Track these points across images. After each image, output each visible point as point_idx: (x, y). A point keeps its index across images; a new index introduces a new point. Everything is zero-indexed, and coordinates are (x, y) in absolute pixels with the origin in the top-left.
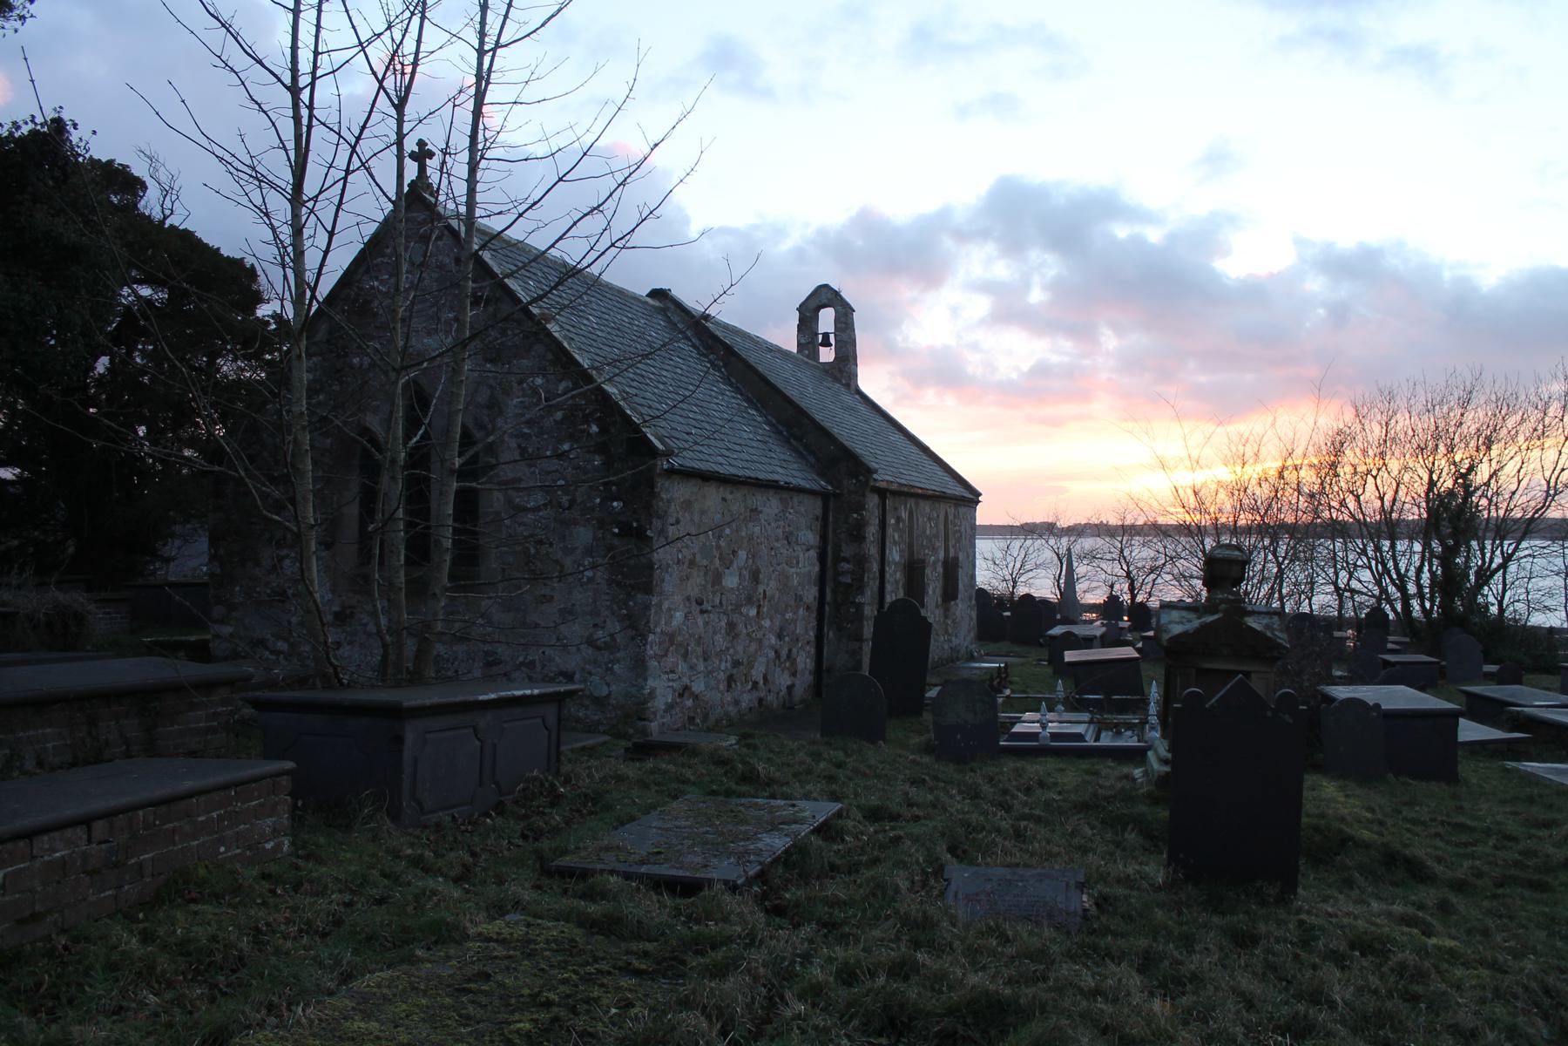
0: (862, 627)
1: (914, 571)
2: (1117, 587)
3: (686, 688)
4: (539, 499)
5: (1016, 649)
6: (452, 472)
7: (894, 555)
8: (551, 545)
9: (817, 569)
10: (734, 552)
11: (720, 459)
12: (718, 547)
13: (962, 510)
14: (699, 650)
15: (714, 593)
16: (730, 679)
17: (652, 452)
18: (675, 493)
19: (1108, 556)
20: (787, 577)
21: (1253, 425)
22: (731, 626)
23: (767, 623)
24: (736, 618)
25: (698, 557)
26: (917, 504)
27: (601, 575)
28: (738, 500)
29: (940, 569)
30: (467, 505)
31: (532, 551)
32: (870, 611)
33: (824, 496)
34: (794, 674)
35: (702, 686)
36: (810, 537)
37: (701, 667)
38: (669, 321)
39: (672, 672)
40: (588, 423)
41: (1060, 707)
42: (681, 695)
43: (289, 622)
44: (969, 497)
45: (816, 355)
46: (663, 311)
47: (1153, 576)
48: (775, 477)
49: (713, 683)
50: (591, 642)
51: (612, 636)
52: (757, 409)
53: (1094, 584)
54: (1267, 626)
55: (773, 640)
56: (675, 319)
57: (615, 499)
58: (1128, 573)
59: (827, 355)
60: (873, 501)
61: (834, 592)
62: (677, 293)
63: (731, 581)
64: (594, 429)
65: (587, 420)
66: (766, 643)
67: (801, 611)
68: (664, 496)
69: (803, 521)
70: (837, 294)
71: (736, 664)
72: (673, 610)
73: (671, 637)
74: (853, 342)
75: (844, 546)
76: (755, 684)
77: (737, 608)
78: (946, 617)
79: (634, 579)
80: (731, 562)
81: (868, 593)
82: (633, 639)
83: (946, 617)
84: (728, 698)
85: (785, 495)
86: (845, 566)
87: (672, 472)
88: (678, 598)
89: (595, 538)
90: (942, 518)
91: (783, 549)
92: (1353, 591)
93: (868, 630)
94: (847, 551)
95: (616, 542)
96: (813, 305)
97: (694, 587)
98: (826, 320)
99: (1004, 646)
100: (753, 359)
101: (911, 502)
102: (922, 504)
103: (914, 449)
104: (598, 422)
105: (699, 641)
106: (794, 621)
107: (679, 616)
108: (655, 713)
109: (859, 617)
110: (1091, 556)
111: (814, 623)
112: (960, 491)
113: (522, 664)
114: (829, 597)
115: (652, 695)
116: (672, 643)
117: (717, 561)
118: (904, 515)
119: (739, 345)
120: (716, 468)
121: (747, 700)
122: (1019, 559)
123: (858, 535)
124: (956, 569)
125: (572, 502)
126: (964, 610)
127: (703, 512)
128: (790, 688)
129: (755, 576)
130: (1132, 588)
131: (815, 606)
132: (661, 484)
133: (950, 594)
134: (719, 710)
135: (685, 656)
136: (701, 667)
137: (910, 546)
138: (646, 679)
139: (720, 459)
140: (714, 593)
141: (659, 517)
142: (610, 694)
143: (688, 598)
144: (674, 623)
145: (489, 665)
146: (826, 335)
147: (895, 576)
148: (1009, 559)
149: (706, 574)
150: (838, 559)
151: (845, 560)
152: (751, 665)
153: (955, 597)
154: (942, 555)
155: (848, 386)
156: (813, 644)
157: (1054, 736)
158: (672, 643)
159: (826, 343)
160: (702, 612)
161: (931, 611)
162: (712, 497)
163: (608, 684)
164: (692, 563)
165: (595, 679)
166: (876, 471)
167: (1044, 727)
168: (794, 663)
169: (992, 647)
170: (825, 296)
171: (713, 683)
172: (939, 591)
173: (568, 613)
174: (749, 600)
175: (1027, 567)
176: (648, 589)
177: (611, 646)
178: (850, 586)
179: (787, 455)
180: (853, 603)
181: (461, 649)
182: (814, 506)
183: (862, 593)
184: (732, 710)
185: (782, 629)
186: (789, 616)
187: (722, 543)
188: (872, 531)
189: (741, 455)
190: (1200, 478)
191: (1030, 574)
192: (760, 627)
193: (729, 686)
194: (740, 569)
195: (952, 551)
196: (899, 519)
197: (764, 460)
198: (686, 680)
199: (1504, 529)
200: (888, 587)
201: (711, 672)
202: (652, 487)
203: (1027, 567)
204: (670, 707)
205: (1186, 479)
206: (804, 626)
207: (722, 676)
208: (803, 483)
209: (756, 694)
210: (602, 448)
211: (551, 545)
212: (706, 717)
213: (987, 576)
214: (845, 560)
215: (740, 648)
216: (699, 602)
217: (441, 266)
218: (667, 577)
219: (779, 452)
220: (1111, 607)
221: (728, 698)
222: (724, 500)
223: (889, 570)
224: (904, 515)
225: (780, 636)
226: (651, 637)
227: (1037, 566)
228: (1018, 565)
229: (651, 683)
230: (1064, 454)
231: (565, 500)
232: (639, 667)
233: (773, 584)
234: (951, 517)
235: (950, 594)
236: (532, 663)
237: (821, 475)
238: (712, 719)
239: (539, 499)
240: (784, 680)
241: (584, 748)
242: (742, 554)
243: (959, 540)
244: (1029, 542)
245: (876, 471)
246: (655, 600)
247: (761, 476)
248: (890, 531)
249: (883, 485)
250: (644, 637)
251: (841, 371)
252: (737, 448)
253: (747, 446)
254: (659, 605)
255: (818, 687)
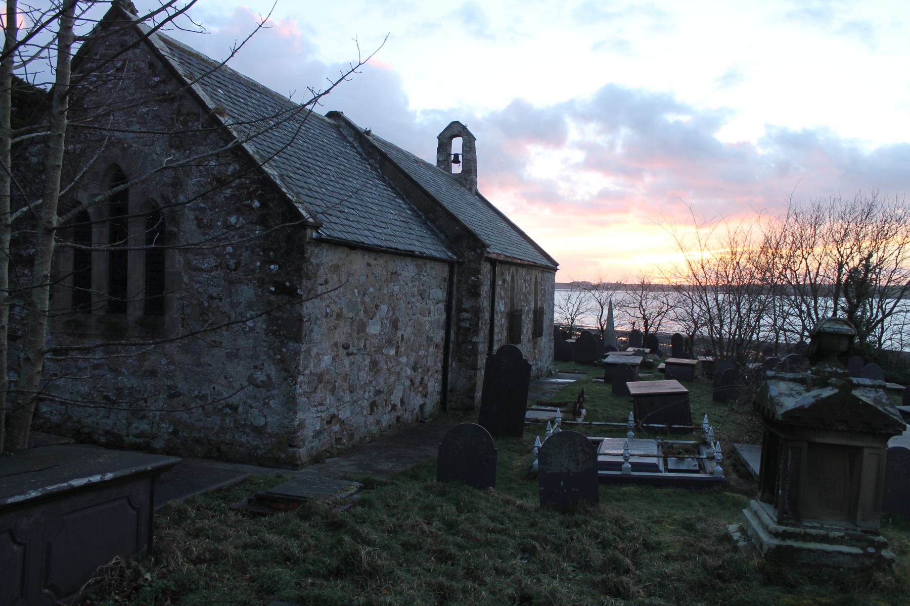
0: (476, 360)
1: (514, 318)
2: (637, 323)
3: (333, 416)
4: (211, 261)
5: (579, 367)
6: (7, 226)
7: (501, 306)
8: (220, 299)
9: (444, 317)
10: (377, 306)
11: (367, 233)
12: (363, 303)
13: (546, 275)
14: (346, 385)
15: (359, 339)
16: (373, 405)
17: (305, 225)
18: (324, 259)
19: (632, 305)
20: (421, 325)
21: (722, 230)
22: (374, 364)
23: (404, 360)
24: (378, 357)
25: (345, 311)
26: (517, 271)
27: (261, 325)
28: (380, 265)
29: (531, 316)
30: (156, 264)
31: (206, 304)
32: (482, 348)
33: (451, 264)
34: (425, 396)
35: (348, 414)
36: (440, 294)
37: (347, 398)
38: (341, 134)
39: (321, 404)
40: (252, 199)
41: (631, 433)
42: (329, 423)
43: (19, 358)
44: (552, 266)
45: (449, 169)
46: (337, 128)
47: (659, 317)
48: (412, 248)
49: (358, 409)
50: (251, 381)
51: (269, 377)
52: (403, 199)
53: (623, 322)
54: (875, 400)
55: (409, 372)
56: (345, 133)
57: (273, 263)
58: (644, 316)
59: (457, 169)
60: (486, 267)
61: (457, 334)
62: (347, 115)
63: (374, 329)
64: (256, 204)
65: (250, 196)
66: (403, 374)
67: (431, 349)
68: (313, 260)
69: (434, 281)
70: (464, 128)
71: (378, 393)
72: (321, 352)
73: (320, 377)
74: (475, 161)
75: (464, 300)
76: (394, 407)
77: (379, 350)
78: (535, 348)
79: (288, 330)
80: (374, 314)
81: (482, 335)
82: (285, 379)
83: (535, 348)
84: (371, 419)
85: (420, 262)
86: (465, 315)
87: (320, 241)
88: (326, 345)
89: (256, 295)
90: (533, 280)
91: (419, 302)
92: (785, 331)
93: (482, 361)
94: (467, 304)
95: (273, 298)
96: (448, 134)
97: (340, 337)
98: (457, 145)
99: (572, 365)
100: (403, 165)
101: (513, 269)
102: (520, 270)
103: (515, 233)
104: (260, 198)
105: (346, 377)
106: (426, 357)
107: (327, 359)
108: (303, 441)
109: (474, 352)
110: (622, 305)
111: (441, 357)
112: (545, 262)
113: (197, 397)
114: (452, 338)
115: (301, 425)
116: (320, 381)
117: (362, 314)
118: (508, 278)
119: (392, 155)
120: (362, 239)
121: (387, 419)
122: (576, 305)
123: (475, 293)
124: (540, 315)
125: (238, 264)
126: (546, 343)
127: (349, 275)
128: (422, 407)
129: (395, 325)
130: (646, 325)
131: (442, 344)
132: (309, 250)
133: (537, 332)
134: (363, 430)
135: (333, 391)
136: (347, 398)
137: (512, 300)
138: (295, 413)
139: (367, 233)
140: (359, 339)
141: (309, 278)
142: (266, 424)
143: (336, 345)
144: (323, 365)
145: (171, 396)
146: (456, 156)
147: (501, 321)
148: (570, 305)
149: (351, 324)
150: (460, 310)
151: (466, 310)
152: (390, 393)
153: (541, 335)
154: (533, 306)
155: (470, 189)
156: (440, 372)
157: (636, 466)
158: (320, 381)
159: (456, 161)
160: (348, 354)
161: (525, 348)
162: (358, 262)
163: (265, 416)
164: (339, 316)
165: (255, 411)
166: (488, 246)
167: (626, 459)
168: (425, 387)
169: (563, 366)
170: (456, 129)
171: (358, 409)
172: (530, 331)
173: (233, 356)
174: (390, 343)
175: (581, 311)
176: (298, 337)
177: (267, 385)
178: (469, 329)
179: (424, 233)
180: (471, 342)
181: (149, 383)
182: (443, 271)
183: (477, 335)
184: (374, 429)
185: (416, 363)
186: (421, 353)
187: (367, 299)
188: (485, 289)
189: (385, 231)
190: (707, 255)
191: (583, 315)
192: (399, 363)
193: (372, 410)
194: (382, 319)
195: (539, 303)
196: (504, 281)
197: (404, 235)
198: (333, 410)
199: (884, 293)
200: (496, 330)
201: (355, 402)
202: (303, 253)
203: (581, 311)
204: (318, 434)
205: (696, 256)
206: (433, 359)
207: (366, 403)
208: (435, 254)
209: (394, 414)
210: (263, 221)
211: (220, 299)
212: (351, 436)
213: (559, 317)
214: (466, 310)
215: (381, 381)
216: (346, 347)
217: (137, 70)
218: (316, 329)
219: (417, 230)
220: (634, 336)
221: (371, 419)
222: (369, 265)
223: (497, 318)
224: (508, 278)
225: (414, 369)
226: (300, 378)
227: (587, 310)
228: (575, 310)
229: (300, 415)
230: (610, 242)
231: (232, 262)
232: (291, 402)
233: (409, 330)
234: (539, 280)
235: (537, 332)
236: (205, 396)
237: (449, 248)
238: (357, 438)
239: (211, 261)
240: (417, 401)
241: (219, 490)
242: (384, 308)
243: (544, 295)
244: (582, 295)
245: (488, 246)
246: (304, 347)
247: (400, 247)
248: (498, 290)
249: (494, 256)
250: (294, 378)
251: (466, 180)
252: (384, 225)
253: (395, 225)
254: (308, 351)
255: (443, 403)
